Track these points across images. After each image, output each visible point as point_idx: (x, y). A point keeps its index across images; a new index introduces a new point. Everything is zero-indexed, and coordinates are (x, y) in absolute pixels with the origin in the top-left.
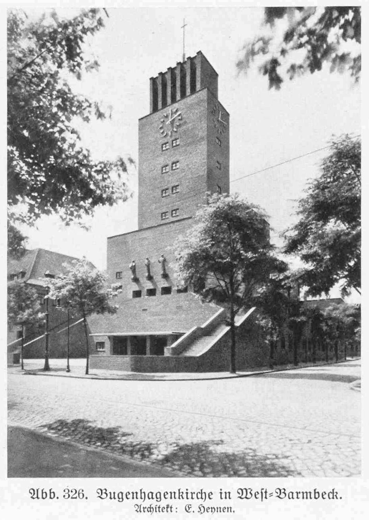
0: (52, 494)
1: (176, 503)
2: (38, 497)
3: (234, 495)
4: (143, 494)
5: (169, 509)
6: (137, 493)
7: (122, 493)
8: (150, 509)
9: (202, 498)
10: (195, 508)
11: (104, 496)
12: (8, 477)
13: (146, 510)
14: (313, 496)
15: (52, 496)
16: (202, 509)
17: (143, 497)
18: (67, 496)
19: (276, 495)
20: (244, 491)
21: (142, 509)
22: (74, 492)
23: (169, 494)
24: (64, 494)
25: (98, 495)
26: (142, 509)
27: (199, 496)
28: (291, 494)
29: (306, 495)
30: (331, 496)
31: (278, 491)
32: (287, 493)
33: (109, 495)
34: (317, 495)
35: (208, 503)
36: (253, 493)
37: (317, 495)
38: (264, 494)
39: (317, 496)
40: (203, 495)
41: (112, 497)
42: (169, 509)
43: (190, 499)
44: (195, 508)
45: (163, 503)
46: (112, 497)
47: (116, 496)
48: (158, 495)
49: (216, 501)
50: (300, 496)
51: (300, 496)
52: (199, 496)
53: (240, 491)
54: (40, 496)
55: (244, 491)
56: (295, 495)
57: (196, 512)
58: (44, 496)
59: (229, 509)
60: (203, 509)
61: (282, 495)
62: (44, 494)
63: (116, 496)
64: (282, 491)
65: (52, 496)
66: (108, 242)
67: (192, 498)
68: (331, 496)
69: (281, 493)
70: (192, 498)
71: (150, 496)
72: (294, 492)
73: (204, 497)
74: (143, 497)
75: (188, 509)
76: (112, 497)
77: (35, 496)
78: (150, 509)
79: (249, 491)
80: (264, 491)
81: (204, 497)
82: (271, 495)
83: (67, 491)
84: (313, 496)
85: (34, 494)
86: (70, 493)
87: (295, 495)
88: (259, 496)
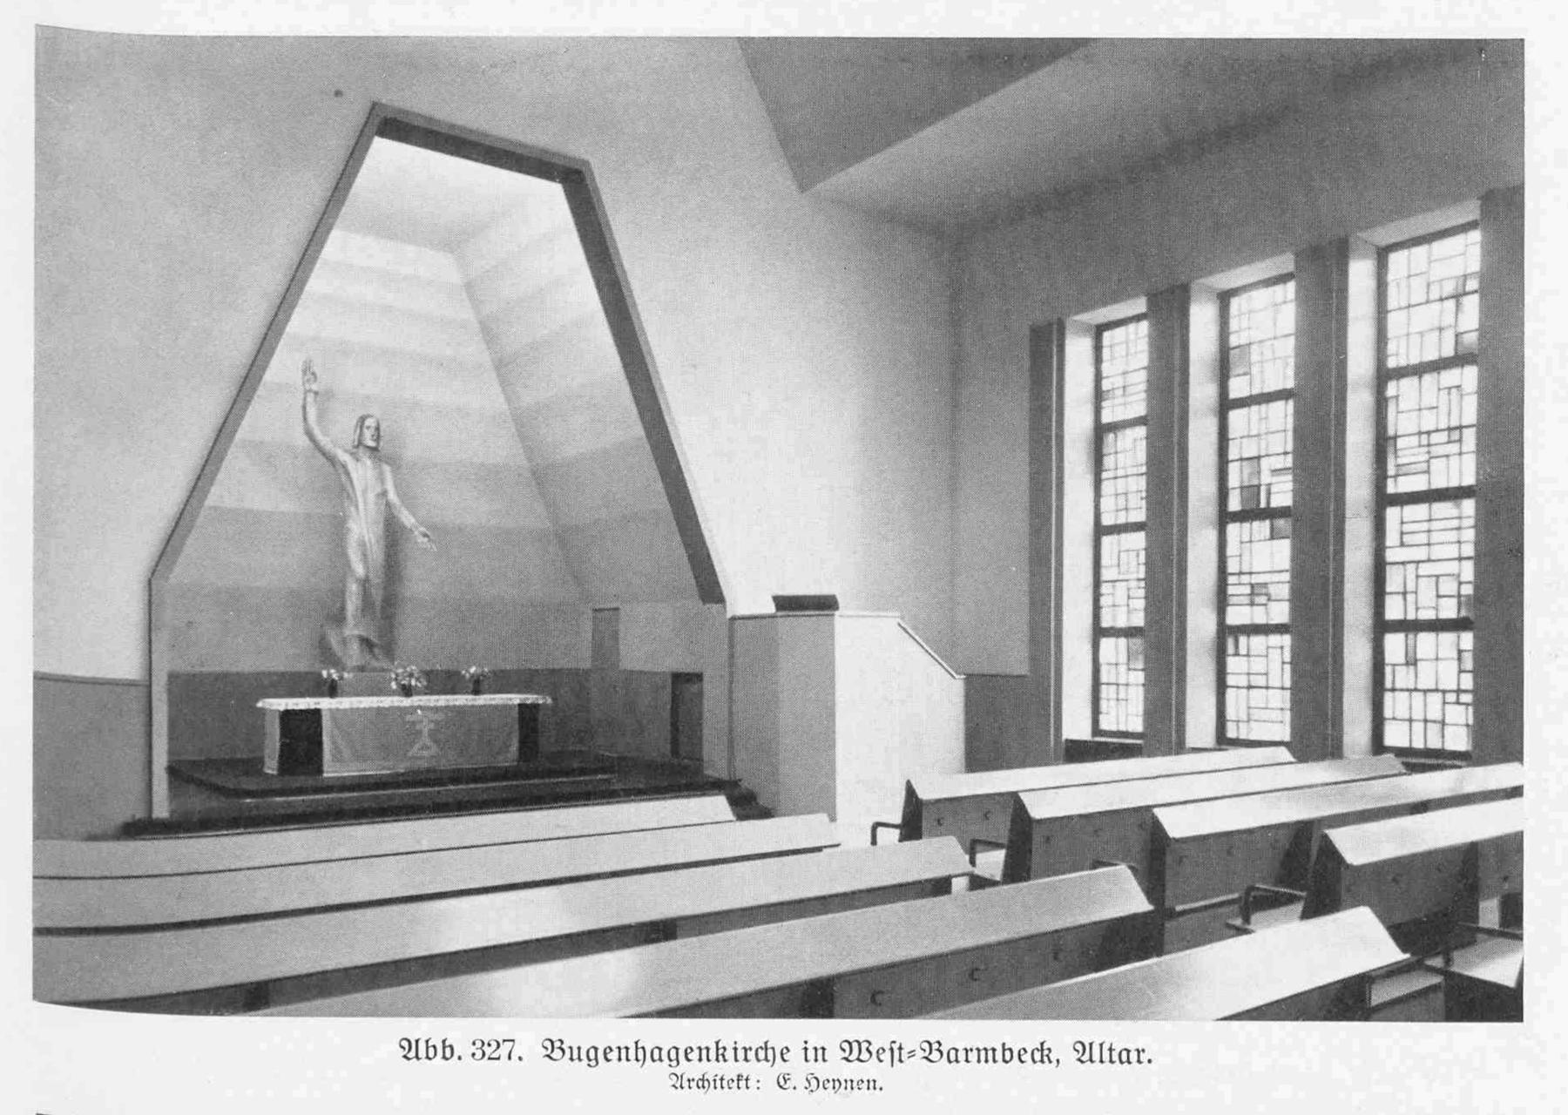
0: (448, 1051)
1: (753, 1069)
2: (417, 1057)
3: (834, 1054)
4: (640, 1052)
5: (742, 1083)
6: (994, 1050)
7: (596, 1049)
8: (703, 1083)
9: (766, 1059)
10: (798, 1080)
11: (557, 1054)
12: (1520, 1019)
13: (693, 1084)
14: (999, 1056)
15: (448, 1054)
16: (814, 1082)
17: (641, 1056)
18: (479, 1054)
19: (920, 1054)
20: (855, 1045)
21: (685, 1084)
22: (494, 1045)
23: (697, 1052)
24: (473, 1049)
25: (545, 1052)
26: (685, 1084)
27: (762, 1054)
28: (953, 1053)
29: (986, 1054)
30: (1037, 1056)
31: (926, 1046)
32: (944, 1049)
33: (568, 1051)
34: (1008, 1054)
35: (822, 1070)
36: (873, 1049)
37: (1008, 1054)
38: (896, 1053)
39: (1008, 1057)
40: (770, 1052)
41: (575, 1055)
42: (742, 1083)
43: (742, 1062)
44: (798, 1080)
45: (730, 1069)
46: (575, 1056)
47: (583, 1056)
48: (592, 1052)
49: (835, 1067)
50: (973, 1056)
51: (973, 1056)
52: (762, 1054)
53: (846, 1046)
54: (422, 1053)
55: (855, 1045)
56: (1133, 1056)
57: (800, 1088)
58: (1008, 1057)
59: (872, 1084)
60: (816, 1083)
61: (935, 1056)
62: (431, 1050)
63: (583, 1056)
64: (935, 1046)
65: (448, 1054)
66: (35, 885)
67: (746, 1059)
68: (1037, 1056)
69: (932, 1049)
70: (746, 1059)
71: (656, 1056)
72: (960, 1047)
73: (770, 1057)
74: (641, 1056)
75: (782, 1082)
76: (575, 1056)
77: (412, 1054)
78: (703, 1083)
79: (864, 1045)
80: (896, 1047)
81: (770, 1057)
82: (912, 1054)
83: (479, 1044)
84: (999, 1056)
85: (410, 1049)
86: (486, 1048)
87: (1133, 1056)
88: (886, 1056)
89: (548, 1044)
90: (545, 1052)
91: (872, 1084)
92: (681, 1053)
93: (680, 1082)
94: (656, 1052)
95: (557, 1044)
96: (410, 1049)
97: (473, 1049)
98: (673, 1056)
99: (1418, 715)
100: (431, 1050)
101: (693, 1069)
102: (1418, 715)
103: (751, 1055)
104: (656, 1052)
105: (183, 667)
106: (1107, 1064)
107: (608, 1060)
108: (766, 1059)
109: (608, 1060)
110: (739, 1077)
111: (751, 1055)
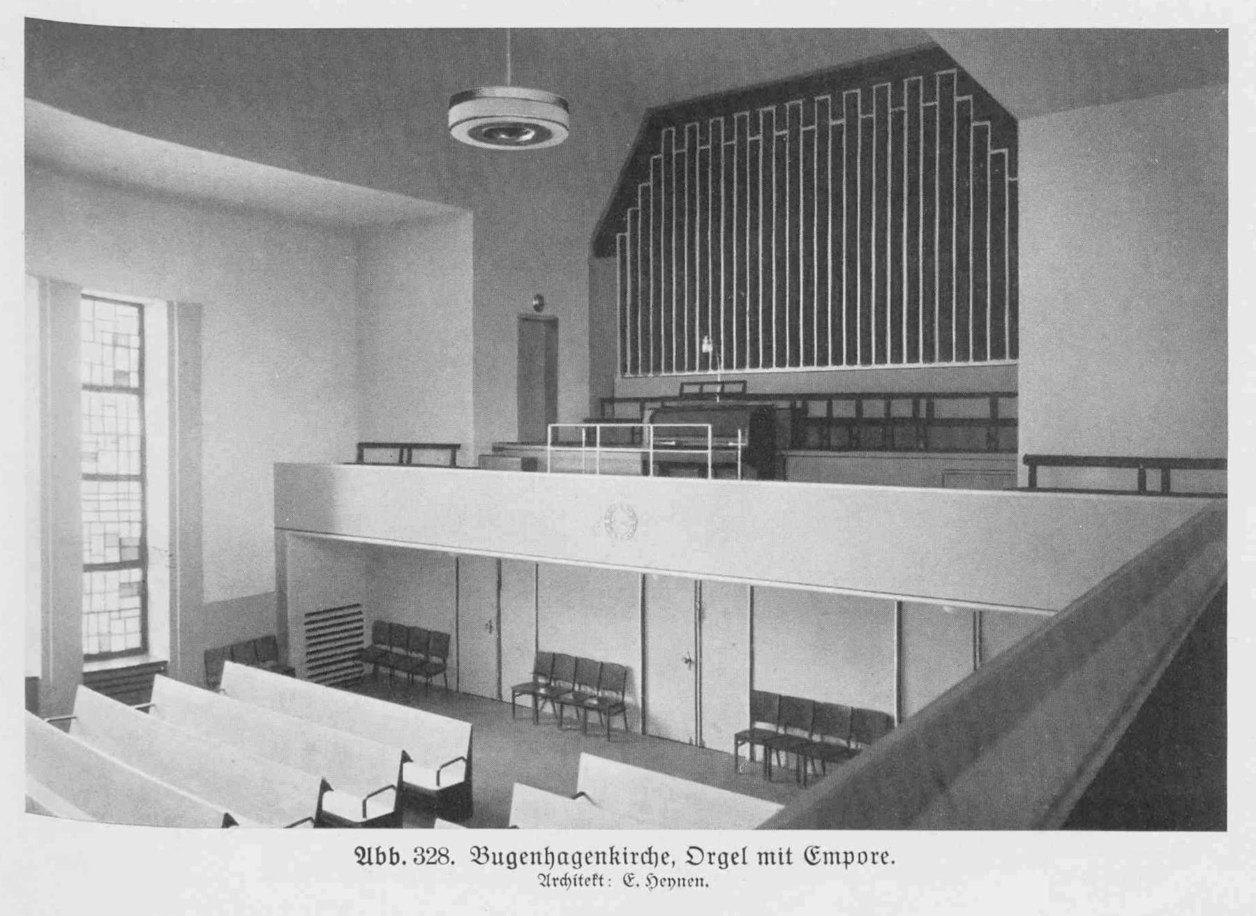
0: (395, 857)
2: (370, 863)
4: (550, 856)
5: (597, 882)
9: (650, 862)
13: (558, 882)
15: (395, 860)
16: (653, 881)
17: (550, 860)
21: (551, 882)
22: (432, 852)
23: (530, 856)
24: (415, 855)
25: (472, 857)
26: (551, 882)
27: (646, 858)
35: (662, 871)
40: (653, 856)
42: (597, 882)
45: (587, 871)
47: (504, 860)
54: (374, 859)
57: (642, 886)
58: (381, 860)
59: (700, 882)
62: (381, 857)
63: (504, 860)
65: (395, 860)
71: (562, 860)
73: (653, 860)
74: (550, 860)
75: (628, 881)
80: (784, 852)
81: (653, 860)
83: (419, 851)
89: (475, 851)
90: (472, 857)
91: (700, 882)
92: (583, 857)
93: (546, 881)
94: (563, 856)
95: (483, 851)
96: (363, 856)
97: (415, 855)
98: (576, 860)
99: (102, 497)
100: (381, 857)
101: (558, 871)
102: (102, 497)
103: (638, 859)
104: (563, 856)
105: (611, 259)
106: (786, 865)
107: (735, 863)
108: (650, 862)
109: (735, 863)
110: (595, 876)
111: (638, 859)
